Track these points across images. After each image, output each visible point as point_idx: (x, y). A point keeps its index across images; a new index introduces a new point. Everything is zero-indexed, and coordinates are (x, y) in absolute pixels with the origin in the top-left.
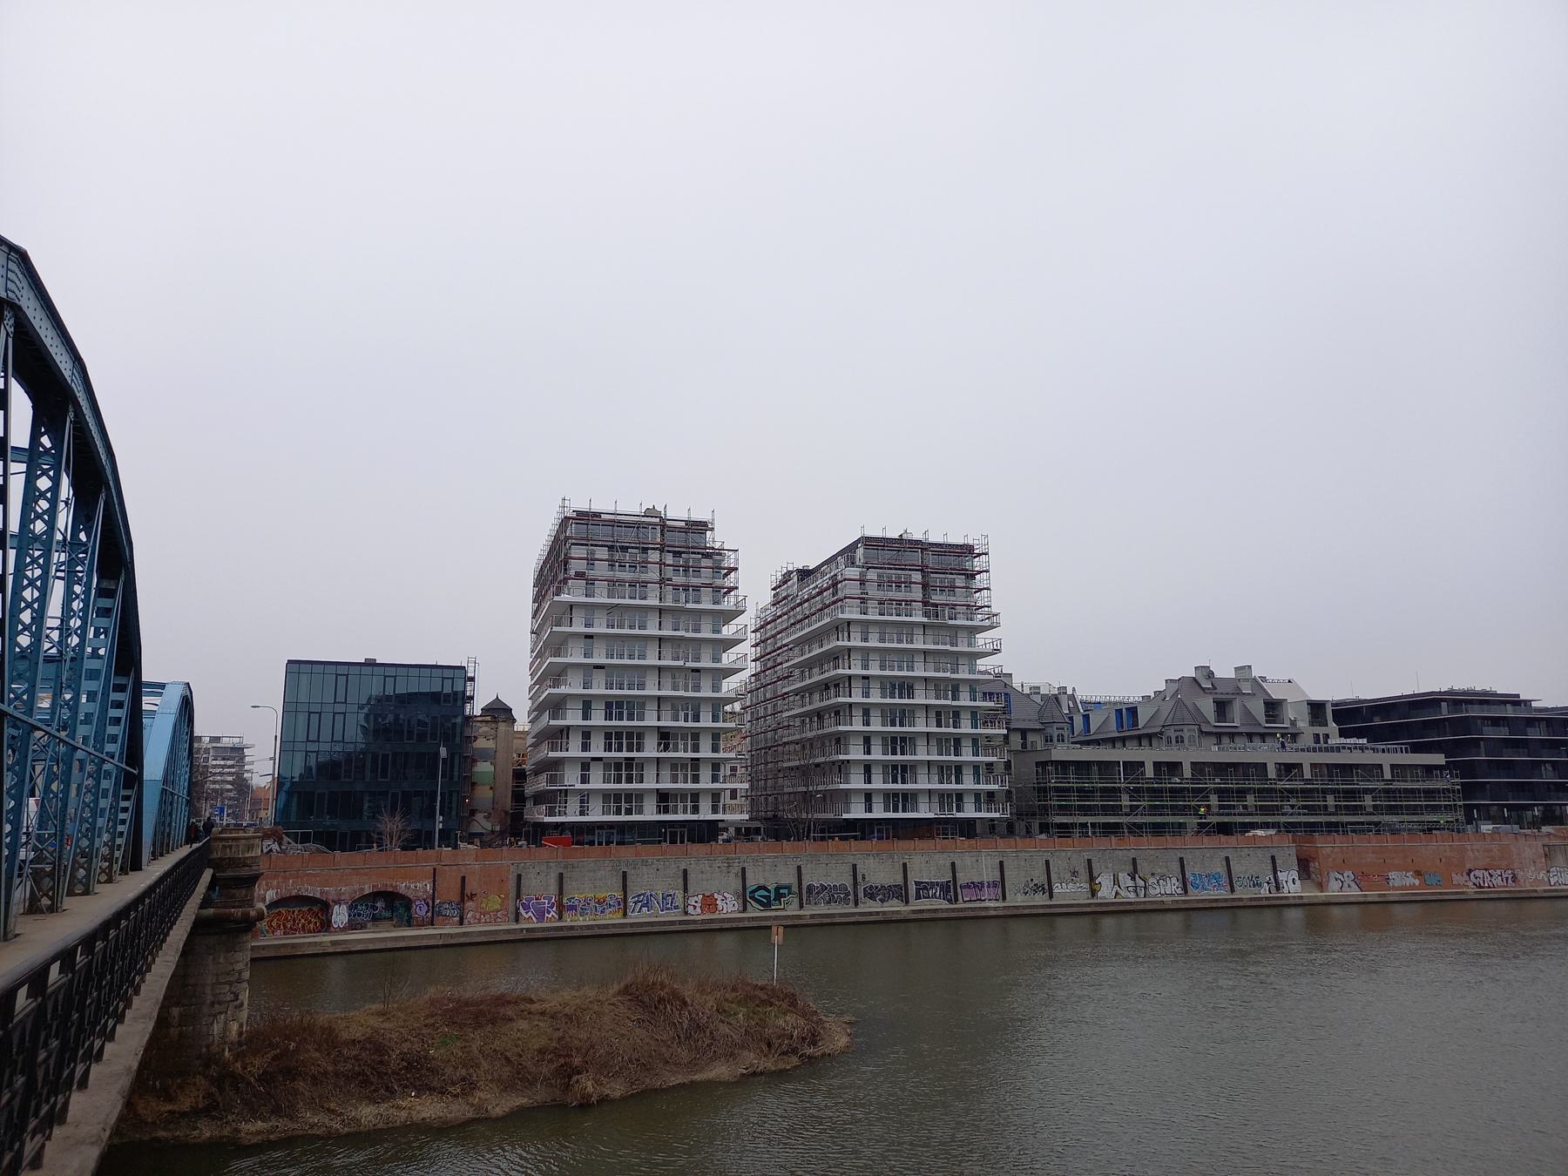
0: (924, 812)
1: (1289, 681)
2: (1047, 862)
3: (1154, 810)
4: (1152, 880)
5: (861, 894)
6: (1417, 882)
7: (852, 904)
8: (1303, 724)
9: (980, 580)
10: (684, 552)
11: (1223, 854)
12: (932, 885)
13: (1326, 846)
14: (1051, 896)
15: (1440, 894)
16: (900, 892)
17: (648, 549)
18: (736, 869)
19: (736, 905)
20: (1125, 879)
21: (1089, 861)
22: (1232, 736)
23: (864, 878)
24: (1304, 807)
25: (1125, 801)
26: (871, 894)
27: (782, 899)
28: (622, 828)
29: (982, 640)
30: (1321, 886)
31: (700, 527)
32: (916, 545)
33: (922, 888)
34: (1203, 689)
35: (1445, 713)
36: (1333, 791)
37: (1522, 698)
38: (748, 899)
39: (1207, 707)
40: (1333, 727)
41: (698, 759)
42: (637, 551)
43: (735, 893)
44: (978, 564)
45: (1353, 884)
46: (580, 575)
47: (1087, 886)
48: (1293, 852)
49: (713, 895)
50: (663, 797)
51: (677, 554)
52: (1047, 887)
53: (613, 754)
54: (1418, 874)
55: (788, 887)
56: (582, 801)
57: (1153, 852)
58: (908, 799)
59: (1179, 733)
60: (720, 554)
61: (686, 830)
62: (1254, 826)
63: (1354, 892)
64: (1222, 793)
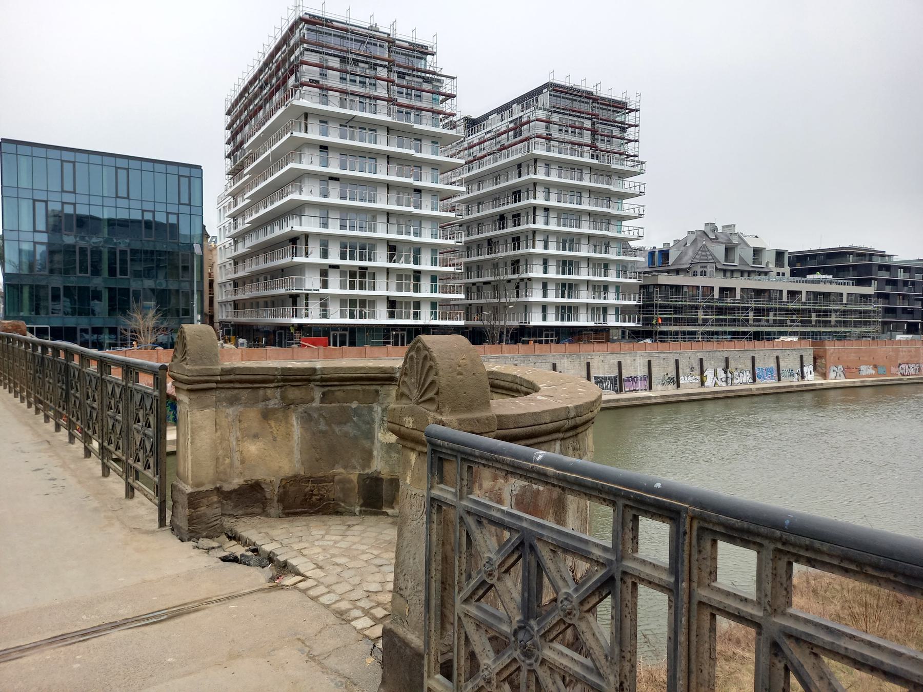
1: (756, 237)
2: (677, 361)
3: (718, 322)
4: (736, 373)
6: (874, 372)
8: (772, 266)
9: (631, 133)
10: (407, 74)
11: (775, 354)
13: (832, 348)
14: (678, 386)
15: (891, 380)
17: (376, 65)
20: (721, 374)
21: (701, 360)
22: (732, 272)
24: (802, 321)
25: (701, 315)
28: (352, 329)
29: (628, 185)
30: (824, 376)
31: (422, 51)
32: (589, 97)
34: (711, 239)
35: (851, 260)
36: (816, 311)
37: (886, 253)
39: (719, 251)
40: (787, 269)
41: (419, 272)
42: (367, 66)
44: (630, 118)
45: (842, 375)
46: (314, 83)
47: (698, 378)
48: (811, 352)
50: (392, 303)
51: (401, 75)
52: (675, 380)
53: (348, 262)
54: (875, 367)
56: (322, 305)
57: (737, 353)
59: (703, 269)
60: (439, 81)
61: (405, 333)
63: (842, 380)
64: (758, 311)
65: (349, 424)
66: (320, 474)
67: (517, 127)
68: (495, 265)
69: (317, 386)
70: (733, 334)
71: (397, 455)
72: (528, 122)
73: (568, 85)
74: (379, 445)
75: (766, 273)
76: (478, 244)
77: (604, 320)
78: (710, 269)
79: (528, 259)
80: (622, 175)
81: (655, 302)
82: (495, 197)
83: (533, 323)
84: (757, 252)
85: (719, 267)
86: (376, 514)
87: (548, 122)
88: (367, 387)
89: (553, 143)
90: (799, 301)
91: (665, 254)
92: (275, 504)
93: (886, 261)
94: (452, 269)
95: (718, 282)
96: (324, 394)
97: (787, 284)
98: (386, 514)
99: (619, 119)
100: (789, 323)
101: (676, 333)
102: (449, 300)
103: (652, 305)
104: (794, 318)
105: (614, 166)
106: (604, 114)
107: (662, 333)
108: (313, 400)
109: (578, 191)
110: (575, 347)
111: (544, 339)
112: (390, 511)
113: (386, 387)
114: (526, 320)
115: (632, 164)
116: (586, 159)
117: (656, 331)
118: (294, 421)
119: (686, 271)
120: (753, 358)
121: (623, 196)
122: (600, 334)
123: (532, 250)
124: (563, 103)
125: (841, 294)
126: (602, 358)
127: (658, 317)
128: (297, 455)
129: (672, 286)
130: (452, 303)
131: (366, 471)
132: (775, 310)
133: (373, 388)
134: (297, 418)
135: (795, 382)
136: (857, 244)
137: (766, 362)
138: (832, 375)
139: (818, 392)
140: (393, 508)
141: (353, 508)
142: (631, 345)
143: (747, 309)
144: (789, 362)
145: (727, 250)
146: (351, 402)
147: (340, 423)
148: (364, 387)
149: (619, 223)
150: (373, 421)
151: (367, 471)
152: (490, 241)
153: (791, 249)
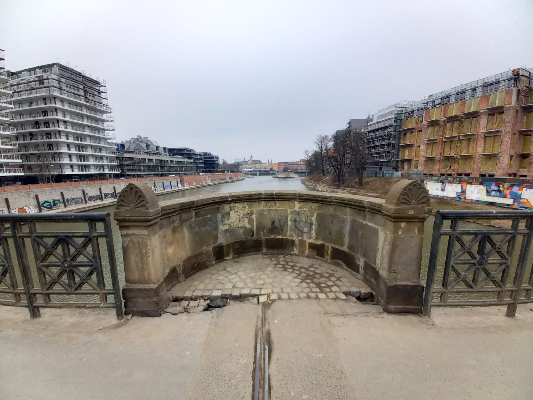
0: (93, 171)
4: (158, 188)
5: (87, 200)
7: (84, 203)
8: (163, 152)
9: (103, 95)
11: (169, 180)
12: (109, 194)
13: (185, 178)
16: (100, 197)
18: (32, 195)
19: (36, 210)
22: (150, 153)
23: (87, 194)
25: (142, 168)
26: (91, 199)
27: (57, 205)
29: (105, 116)
30: (184, 186)
32: (80, 74)
33: (107, 196)
35: (185, 152)
36: (178, 167)
38: (42, 207)
39: (144, 146)
40: (167, 153)
43: (35, 206)
44: (102, 89)
48: (179, 179)
49: (23, 208)
54: (196, 182)
55: (58, 200)
58: (86, 167)
59: (140, 152)
62: (170, 174)
63: (188, 187)
64: (162, 167)
65: (207, 226)
66: (198, 252)
67: (41, 80)
68: (37, 146)
69: (194, 210)
70: (154, 174)
71: (229, 234)
72: (48, 79)
73: (68, 66)
74: (221, 232)
75: (161, 154)
76: (24, 136)
77: (62, 171)
78: (142, 152)
79: (58, 144)
80: (102, 112)
81: (124, 164)
82: (31, 113)
83: (66, 173)
84: (157, 147)
85: (145, 151)
86: (222, 261)
87: (59, 82)
88: (214, 207)
89: (63, 91)
90: (174, 164)
91: (123, 146)
92: (182, 275)
93: (194, 153)
94: (11, 147)
95: (147, 157)
96: (196, 213)
97: (169, 158)
98: (227, 260)
99: (97, 88)
100: (171, 171)
101: (135, 175)
102: (8, 163)
103: (123, 165)
104: (173, 169)
105: (98, 108)
106: (89, 84)
107: (128, 175)
108: (192, 218)
109: (82, 116)
110: (92, 182)
111: (73, 180)
112: (228, 258)
113: (222, 205)
114: (62, 171)
115: (106, 108)
116: (83, 102)
117: (126, 175)
118: (186, 231)
119: (133, 152)
120: (163, 182)
121: (103, 121)
122: (102, 177)
123: (60, 140)
124: (66, 74)
125: (185, 162)
126: (106, 186)
127: (126, 169)
128: (188, 248)
129: (129, 158)
130: (10, 164)
131: (216, 245)
132: (167, 166)
133: (217, 206)
134: (186, 229)
135: (176, 189)
136: (186, 147)
137: (167, 183)
138: (186, 186)
139: (183, 191)
140: (229, 256)
141: (212, 263)
142: (118, 180)
143: (158, 166)
144: (174, 183)
145: (147, 146)
146: (207, 215)
147: (203, 226)
148: (213, 207)
149: (103, 132)
150: (217, 222)
151: (216, 244)
152: (31, 134)
153: (168, 148)
